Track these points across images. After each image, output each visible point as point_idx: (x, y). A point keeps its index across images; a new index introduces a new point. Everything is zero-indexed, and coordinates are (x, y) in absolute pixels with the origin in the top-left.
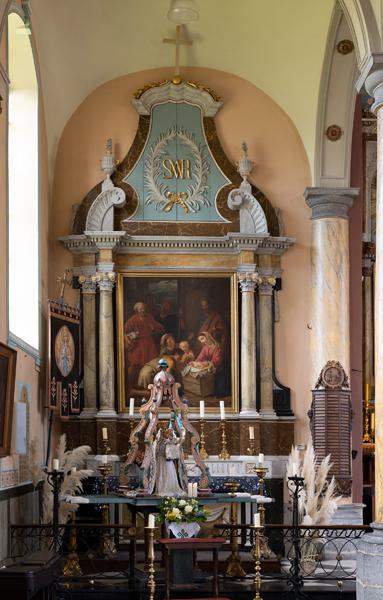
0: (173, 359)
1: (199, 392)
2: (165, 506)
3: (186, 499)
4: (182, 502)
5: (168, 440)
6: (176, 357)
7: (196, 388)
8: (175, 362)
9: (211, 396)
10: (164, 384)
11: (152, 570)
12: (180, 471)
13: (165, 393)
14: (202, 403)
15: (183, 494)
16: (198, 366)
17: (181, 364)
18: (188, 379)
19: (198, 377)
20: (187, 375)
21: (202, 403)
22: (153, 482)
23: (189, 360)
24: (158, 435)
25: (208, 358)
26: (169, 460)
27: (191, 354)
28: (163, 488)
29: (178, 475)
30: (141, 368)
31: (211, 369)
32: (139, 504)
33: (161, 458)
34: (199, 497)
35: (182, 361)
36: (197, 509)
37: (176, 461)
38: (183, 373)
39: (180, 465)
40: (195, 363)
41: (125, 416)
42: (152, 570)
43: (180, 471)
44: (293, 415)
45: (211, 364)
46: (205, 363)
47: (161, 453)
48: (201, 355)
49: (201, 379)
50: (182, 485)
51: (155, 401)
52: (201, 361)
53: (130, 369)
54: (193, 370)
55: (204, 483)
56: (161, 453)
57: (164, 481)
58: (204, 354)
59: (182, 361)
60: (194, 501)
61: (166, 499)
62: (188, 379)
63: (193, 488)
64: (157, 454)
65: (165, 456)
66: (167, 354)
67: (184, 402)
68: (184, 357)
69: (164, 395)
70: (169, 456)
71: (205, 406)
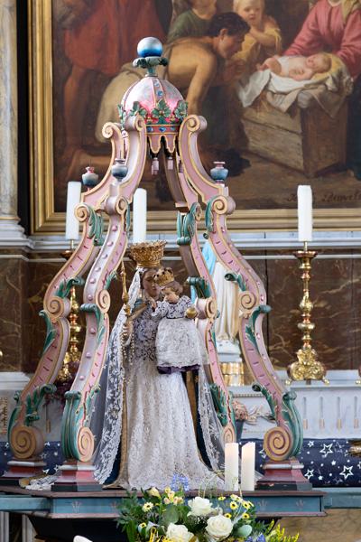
0: (211, 49)
1: (296, 159)
2: (142, 517)
3: (212, 496)
4: (200, 506)
5: (165, 304)
6: (223, 42)
7: (286, 144)
8: (219, 61)
9: (337, 169)
10: (155, 118)
11: (306, 304)
12: (205, 406)
13: (156, 150)
14: (305, 194)
15: (206, 479)
16: (295, 73)
17: (237, 66)
18: (262, 116)
19: (291, 111)
20: (257, 103)
21: (305, 194)
22: (114, 444)
23: (264, 52)
24: (134, 292)
25: (327, 42)
26: (166, 371)
27: (271, 32)
28: (143, 467)
29: (197, 419)
30: (111, 78)
31: (338, 80)
32: (56, 515)
33: (140, 365)
34: (263, 491)
35: (243, 54)
36: (247, 529)
37: (190, 374)
38: (245, 97)
39: (205, 388)
40: (286, 62)
41: (52, 243)
42: (306, 304)
43: (205, 406)
44: (247, 260)
45: (337, 63)
46: (319, 59)
47: (141, 351)
48: (304, 35)
49: (306, 113)
50: (207, 451)
51: (120, 175)
52: (305, 52)
53: (71, 86)
54: (279, 84)
55: (277, 449)
56: (141, 351)
57: (149, 441)
58: (316, 33)
59: (243, 54)
60: (237, 502)
61: (146, 496)
62: (262, 116)
63: (240, 466)
64: (127, 349)
65: (154, 358)
66: (193, 32)
67: (216, 179)
68: (248, 41)
69: (151, 156)
70: (167, 355)
71: (316, 204)
